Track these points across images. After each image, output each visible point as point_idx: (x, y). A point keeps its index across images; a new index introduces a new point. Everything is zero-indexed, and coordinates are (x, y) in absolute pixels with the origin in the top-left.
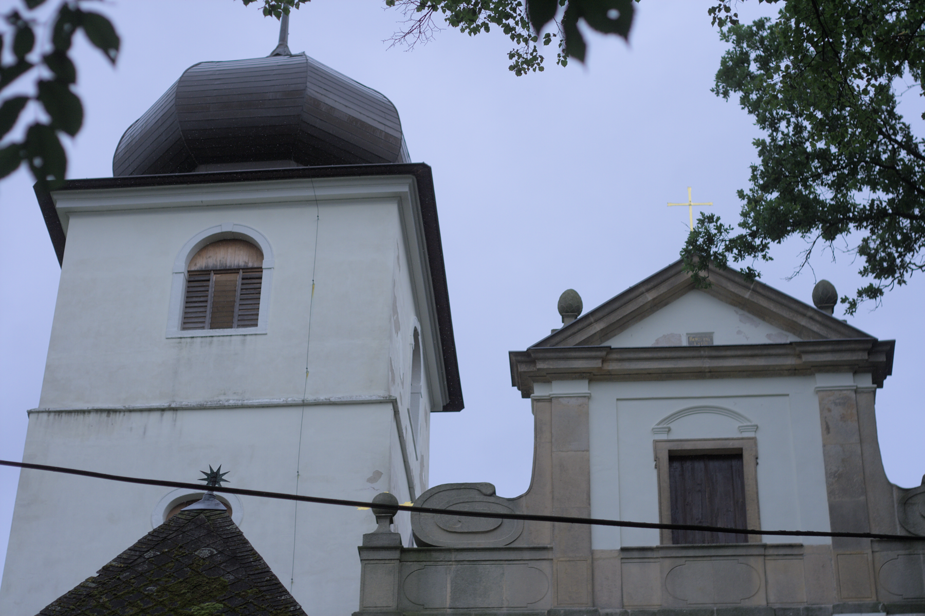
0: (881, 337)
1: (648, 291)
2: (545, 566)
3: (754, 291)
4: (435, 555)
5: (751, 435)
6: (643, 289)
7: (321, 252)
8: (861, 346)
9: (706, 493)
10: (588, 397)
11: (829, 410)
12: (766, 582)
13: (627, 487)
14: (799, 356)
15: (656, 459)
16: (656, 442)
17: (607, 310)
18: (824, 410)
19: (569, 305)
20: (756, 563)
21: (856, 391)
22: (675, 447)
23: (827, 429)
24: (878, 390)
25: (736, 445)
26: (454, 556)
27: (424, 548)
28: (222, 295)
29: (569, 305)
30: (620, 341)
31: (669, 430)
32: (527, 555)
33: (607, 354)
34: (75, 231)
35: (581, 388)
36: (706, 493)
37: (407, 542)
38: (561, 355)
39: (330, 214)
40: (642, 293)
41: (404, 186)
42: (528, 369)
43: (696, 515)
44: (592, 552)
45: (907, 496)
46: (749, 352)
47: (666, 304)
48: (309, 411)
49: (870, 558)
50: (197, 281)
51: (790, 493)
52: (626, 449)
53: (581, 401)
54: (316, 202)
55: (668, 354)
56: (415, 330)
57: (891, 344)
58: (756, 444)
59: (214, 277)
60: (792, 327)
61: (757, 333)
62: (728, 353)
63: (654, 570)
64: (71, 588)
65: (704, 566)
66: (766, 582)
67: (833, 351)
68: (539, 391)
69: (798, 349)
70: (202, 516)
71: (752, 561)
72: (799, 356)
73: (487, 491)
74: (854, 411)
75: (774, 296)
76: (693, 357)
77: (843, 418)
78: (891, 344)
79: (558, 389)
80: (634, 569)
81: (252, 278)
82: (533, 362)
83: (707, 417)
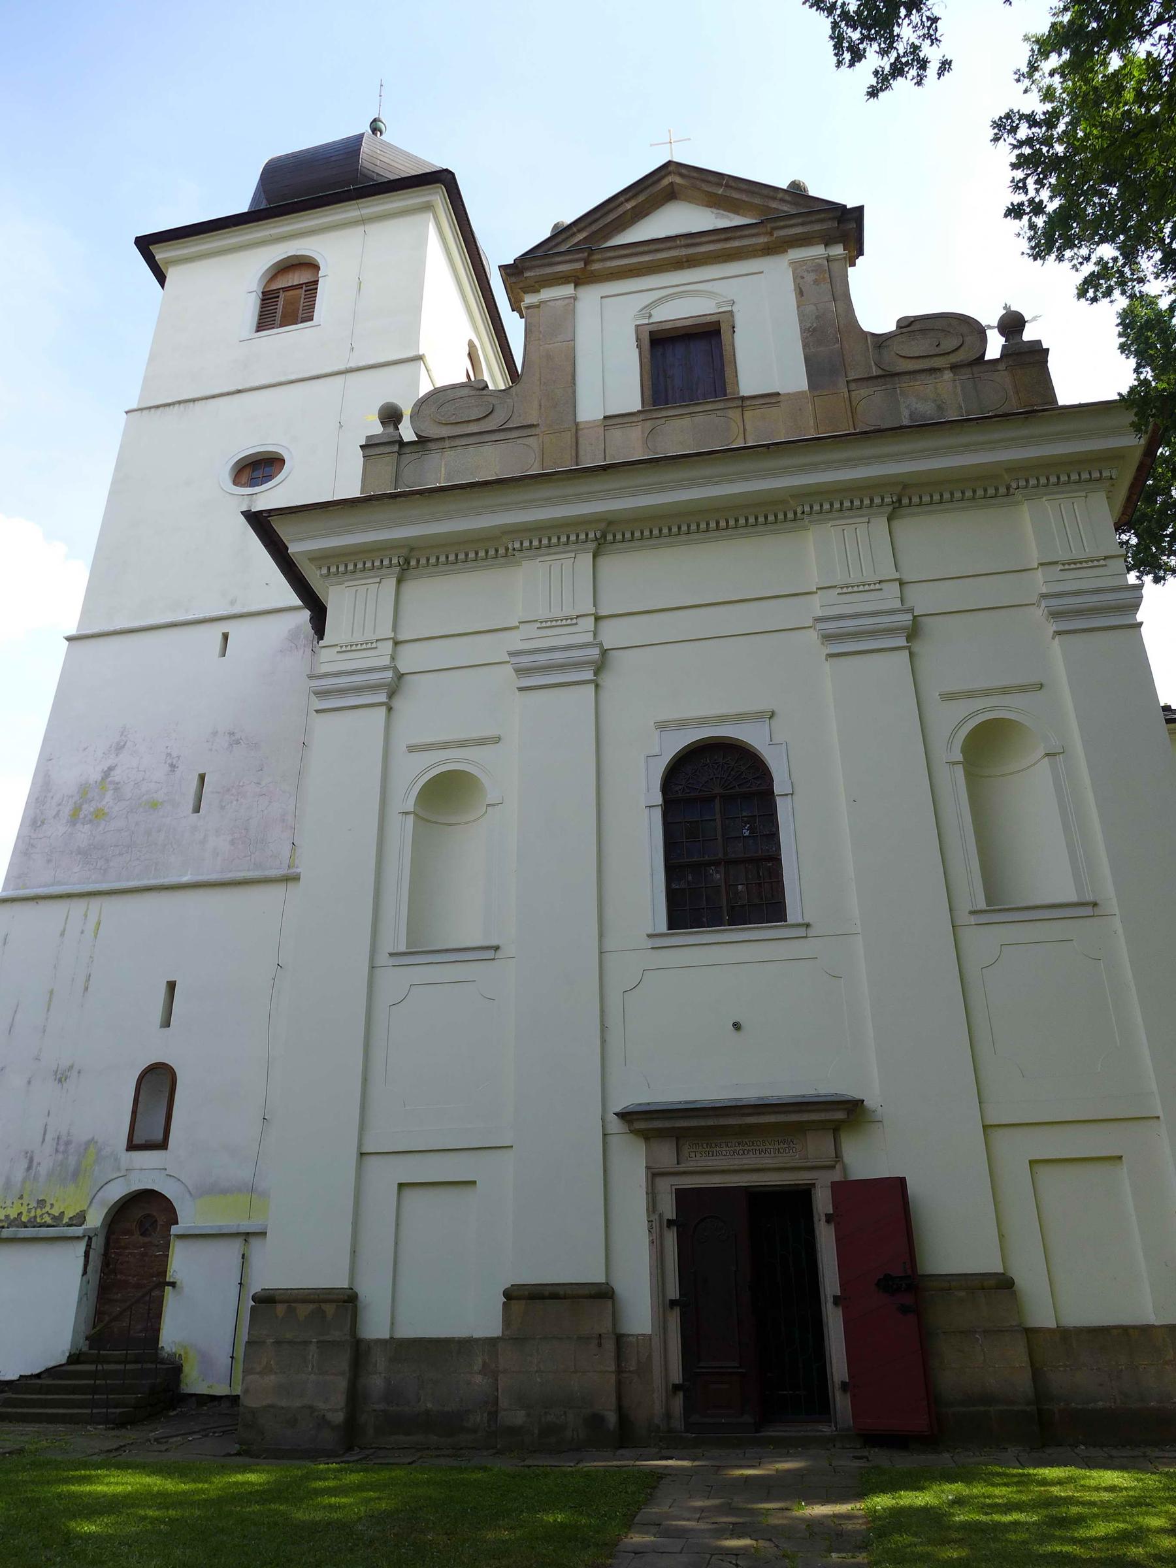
1: (627, 201)
2: (531, 441)
3: (727, 186)
4: (431, 445)
5: (729, 308)
6: (622, 199)
8: (831, 215)
9: (685, 360)
10: (575, 299)
11: (803, 278)
12: (744, 430)
13: (608, 376)
14: (771, 234)
15: (638, 339)
16: (637, 326)
17: (589, 220)
18: (798, 279)
20: (735, 414)
21: (828, 259)
22: (651, 328)
23: (800, 293)
24: (850, 270)
25: (714, 318)
26: (447, 443)
27: (422, 441)
28: (287, 300)
31: (650, 316)
32: (515, 434)
33: (589, 255)
35: (568, 290)
38: (546, 261)
39: (374, 229)
40: (622, 203)
41: (437, 197)
44: (577, 424)
45: (881, 341)
46: (723, 236)
47: (647, 215)
48: (349, 376)
49: (846, 396)
50: (268, 298)
51: (769, 357)
53: (567, 301)
54: (363, 221)
55: (646, 248)
56: (471, 344)
57: (860, 210)
58: (733, 316)
59: (282, 295)
62: (704, 239)
65: (686, 422)
66: (744, 430)
67: (803, 224)
68: (529, 299)
69: (769, 226)
71: (730, 413)
72: (771, 234)
74: (827, 275)
75: (744, 186)
76: (670, 248)
77: (816, 282)
78: (860, 210)
79: (547, 294)
80: (616, 434)
81: (311, 288)
82: (521, 273)
83: (683, 299)
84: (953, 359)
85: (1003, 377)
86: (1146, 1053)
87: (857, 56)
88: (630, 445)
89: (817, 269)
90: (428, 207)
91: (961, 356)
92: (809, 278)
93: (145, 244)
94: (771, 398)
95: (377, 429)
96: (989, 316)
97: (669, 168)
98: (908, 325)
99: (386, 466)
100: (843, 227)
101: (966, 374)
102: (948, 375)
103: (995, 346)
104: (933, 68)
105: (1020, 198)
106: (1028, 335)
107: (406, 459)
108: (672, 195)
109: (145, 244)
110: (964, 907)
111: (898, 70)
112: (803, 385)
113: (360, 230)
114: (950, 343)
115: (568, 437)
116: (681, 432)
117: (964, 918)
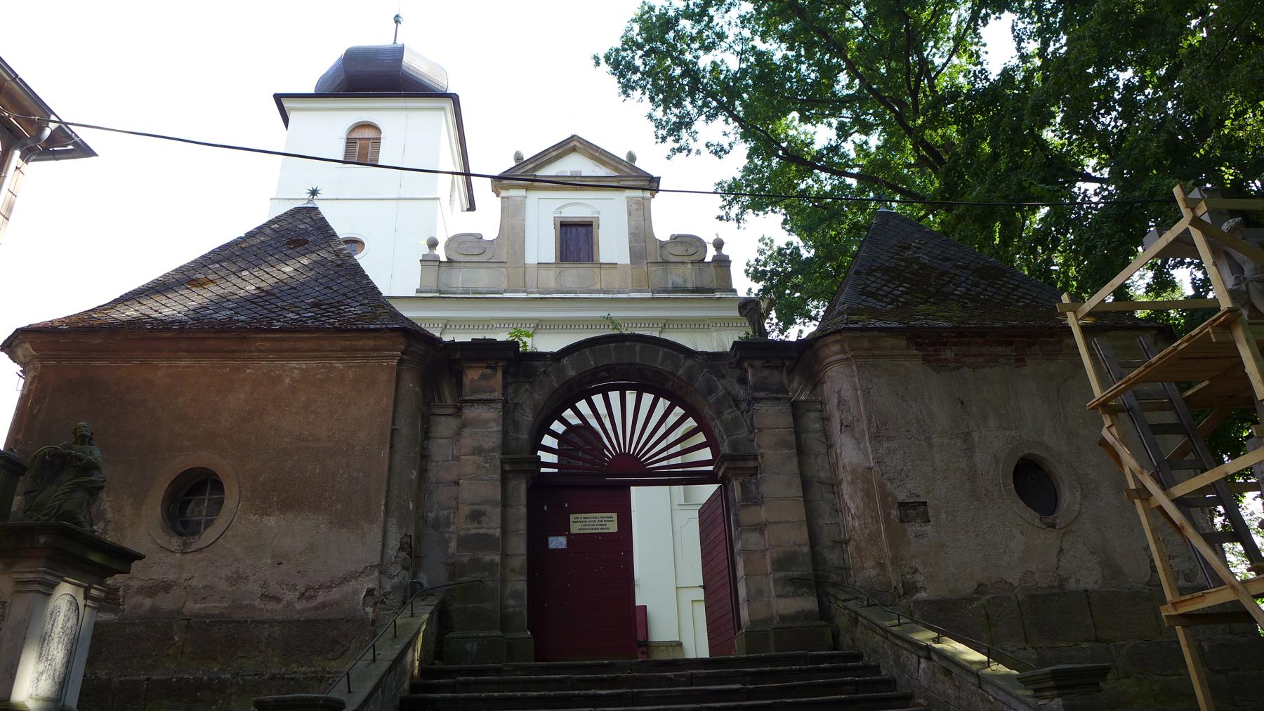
0: (655, 175)
7: (403, 128)
9: (576, 239)
13: (541, 245)
18: (629, 206)
19: (518, 157)
20: (597, 271)
23: (630, 214)
29: (518, 157)
30: (542, 173)
34: (292, 117)
35: (522, 192)
36: (576, 239)
37: (443, 258)
41: (448, 104)
42: (501, 181)
43: (582, 230)
45: (663, 245)
51: (613, 246)
52: (543, 214)
54: (406, 109)
60: (616, 169)
61: (602, 171)
63: (552, 273)
64: (193, 259)
65: (575, 271)
68: (504, 193)
70: (1206, 646)
73: (479, 237)
79: (512, 193)
80: (543, 272)
83: (578, 206)
84: (693, 258)
85: (712, 270)
86: (1189, 660)
87: (664, 139)
88: (549, 279)
89: (638, 202)
90: (443, 109)
91: (694, 258)
92: (634, 207)
93: (278, 98)
94: (613, 265)
95: (426, 250)
96: (709, 239)
97: (573, 138)
98: (676, 239)
99: (433, 272)
100: (652, 184)
101: (697, 266)
102: (690, 266)
103: (711, 253)
104: (694, 151)
105: (723, 213)
106: (725, 251)
107: (442, 269)
108: (574, 150)
109: (278, 98)
110: (676, 502)
111: (680, 150)
112: (627, 261)
113: (405, 113)
114: (692, 250)
115: (521, 271)
116: (574, 275)
117: (675, 507)
